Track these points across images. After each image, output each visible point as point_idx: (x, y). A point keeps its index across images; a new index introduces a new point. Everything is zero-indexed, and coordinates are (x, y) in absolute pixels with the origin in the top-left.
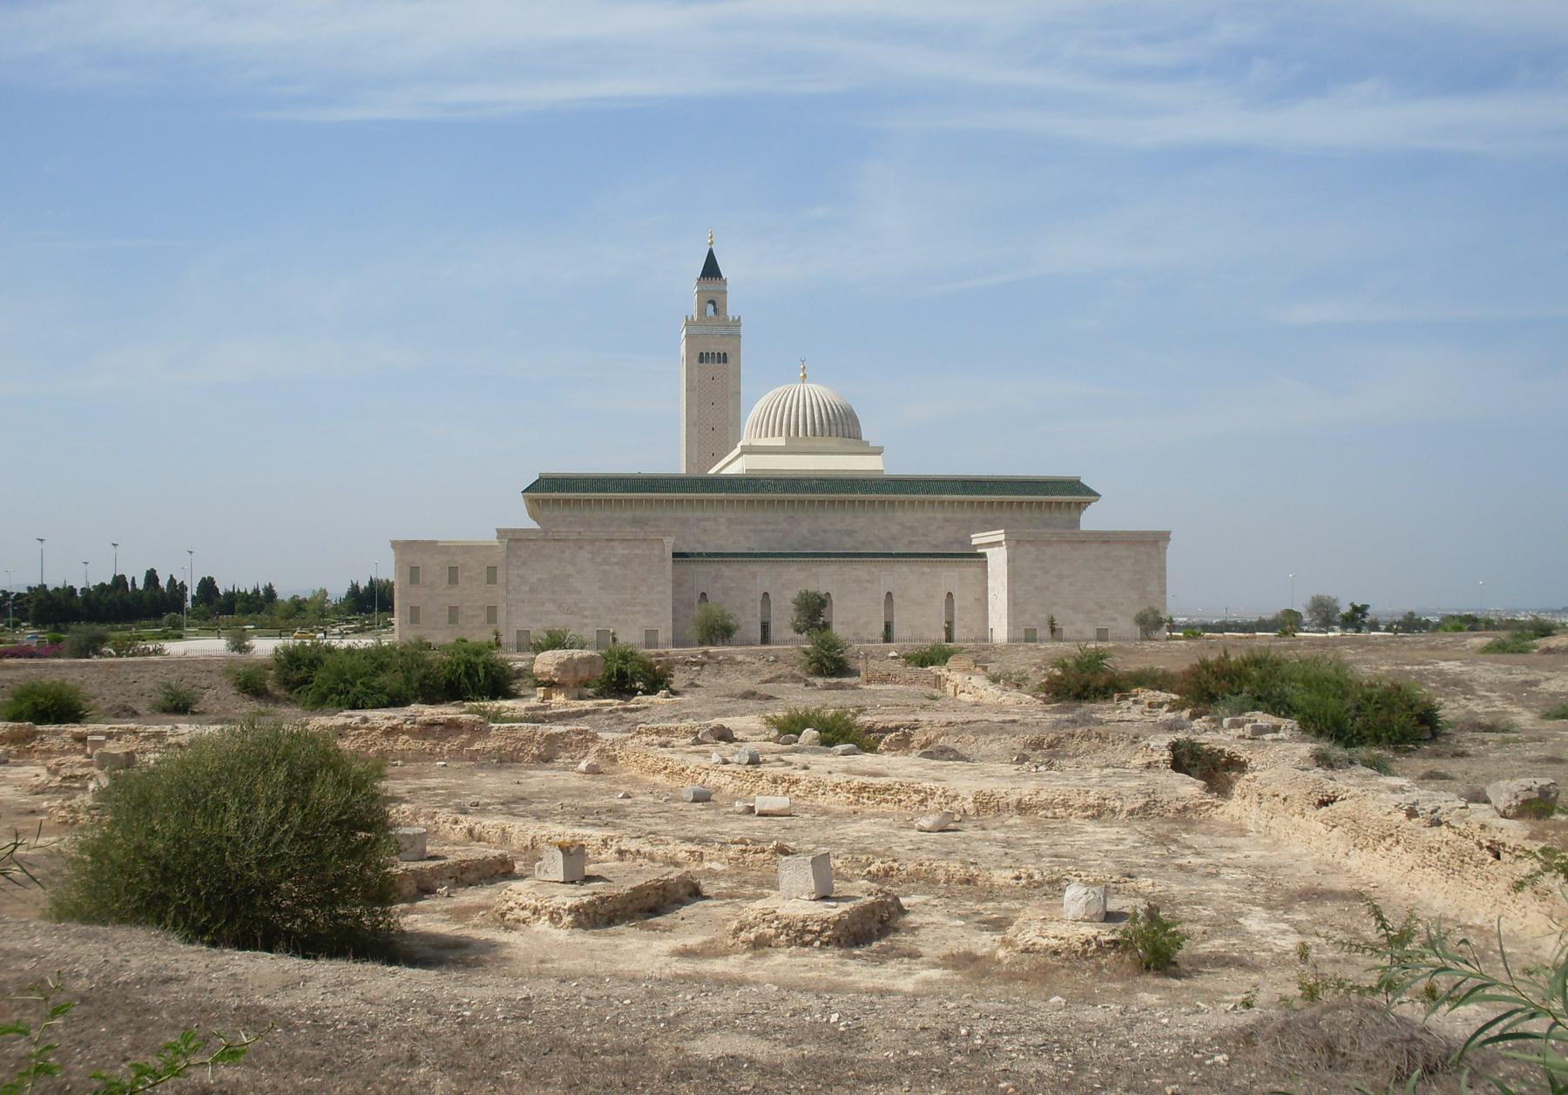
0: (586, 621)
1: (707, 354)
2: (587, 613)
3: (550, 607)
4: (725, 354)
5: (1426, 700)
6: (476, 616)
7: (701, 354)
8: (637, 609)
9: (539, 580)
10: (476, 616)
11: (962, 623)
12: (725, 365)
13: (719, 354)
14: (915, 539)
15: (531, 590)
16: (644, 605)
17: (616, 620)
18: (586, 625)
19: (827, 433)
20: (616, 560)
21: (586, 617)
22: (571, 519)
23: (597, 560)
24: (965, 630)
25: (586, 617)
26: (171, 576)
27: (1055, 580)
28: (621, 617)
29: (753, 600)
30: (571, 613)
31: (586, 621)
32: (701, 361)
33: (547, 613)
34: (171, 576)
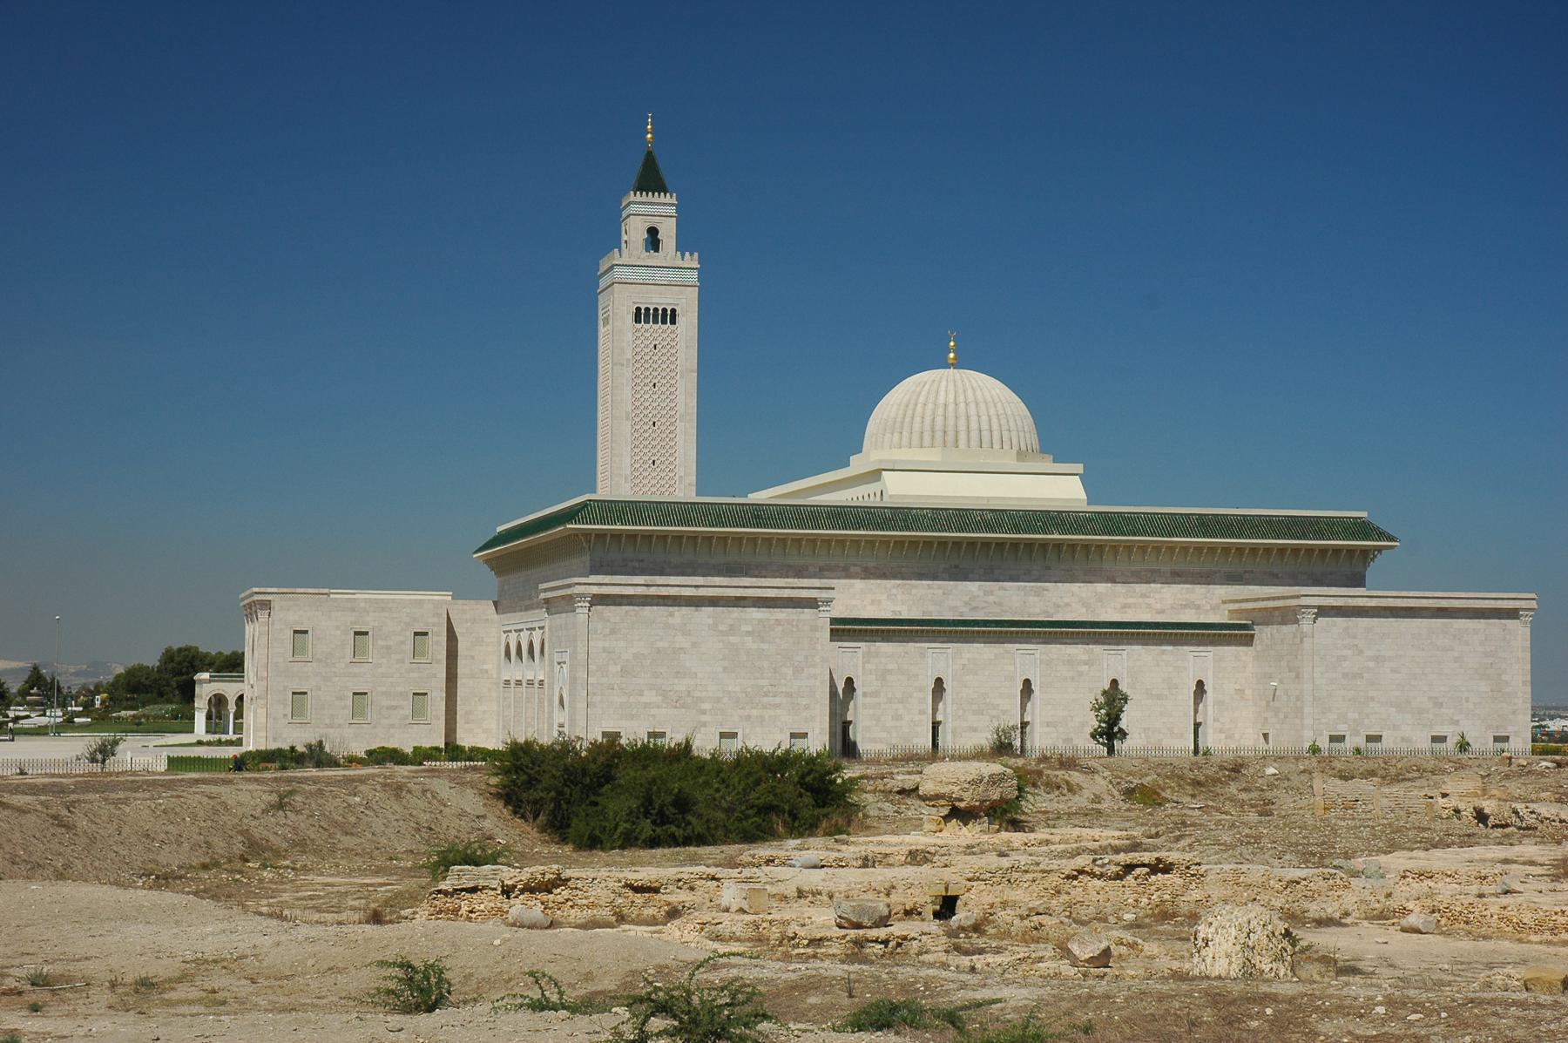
0: (704, 718)
1: (647, 309)
2: (706, 706)
3: (650, 697)
4: (673, 311)
5: (685, 797)
6: (395, 708)
7: (638, 309)
8: (778, 700)
9: (636, 656)
10: (395, 708)
11: (1217, 725)
12: (673, 327)
13: (665, 310)
14: (1130, 600)
15: (624, 672)
16: (789, 695)
17: (749, 717)
18: (705, 725)
19: (997, 446)
20: (749, 628)
21: (704, 712)
22: (637, 564)
23: (721, 628)
24: (1222, 736)
25: (704, 712)
26: (1114, 682)
27: (1372, 664)
28: (755, 712)
29: (920, 689)
30: (682, 707)
31: (704, 718)
32: (637, 319)
33: (647, 705)
34: (1114, 682)
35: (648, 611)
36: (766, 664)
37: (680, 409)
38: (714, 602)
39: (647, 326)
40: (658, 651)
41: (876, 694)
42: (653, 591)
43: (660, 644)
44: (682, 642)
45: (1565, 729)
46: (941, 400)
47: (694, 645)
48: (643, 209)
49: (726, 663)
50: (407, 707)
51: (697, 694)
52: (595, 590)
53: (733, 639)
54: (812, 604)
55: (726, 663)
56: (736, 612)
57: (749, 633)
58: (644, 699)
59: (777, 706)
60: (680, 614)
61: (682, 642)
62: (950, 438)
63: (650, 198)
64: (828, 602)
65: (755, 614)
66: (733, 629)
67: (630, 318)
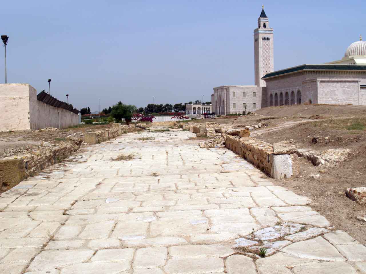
3: (330, 99)
4: (269, 38)
7: (263, 38)
15: (326, 95)
23: (342, 86)
32: (263, 40)
35: (329, 84)
36: (350, 93)
37: (271, 55)
38: (340, 81)
39: (266, 41)
40: (331, 91)
41: (361, 99)
42: (331, 80)
43: (332, 90)
44: (336, 89)
45: (2, 139)
46: (357, 47)
47: (337, 90)
48: (263, 20)
49: (343, 93)
50: (253, 105)
51: (338, 99)
52: (321, 80)
53: (344, 88)
54: (357, 82)
55: (343, 93)
56: (344, 84)
57: (347, 87)
58: (329, 100)
59: (352, 100)
60: (335, 84)
61: (336, 89)
62: (363, 53)
63: (265, 18)
64: (360, 81)
65: (348, 84)
66: (344, 87)
67: (262, 39)
